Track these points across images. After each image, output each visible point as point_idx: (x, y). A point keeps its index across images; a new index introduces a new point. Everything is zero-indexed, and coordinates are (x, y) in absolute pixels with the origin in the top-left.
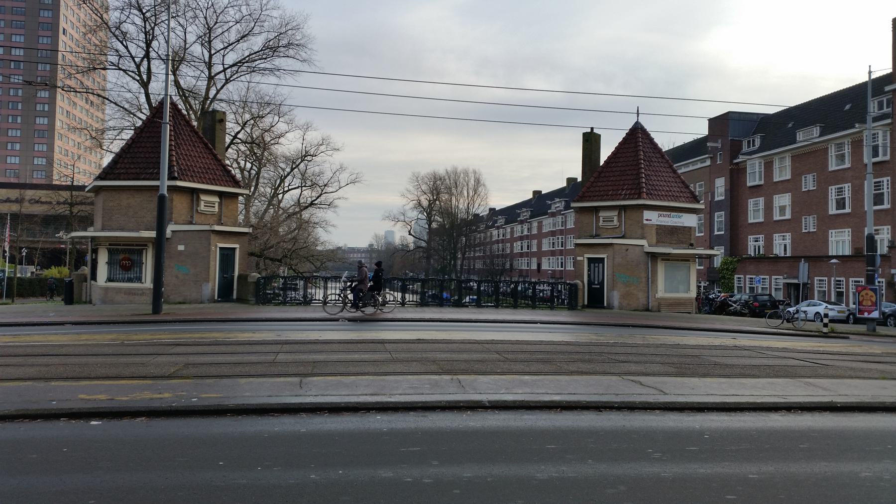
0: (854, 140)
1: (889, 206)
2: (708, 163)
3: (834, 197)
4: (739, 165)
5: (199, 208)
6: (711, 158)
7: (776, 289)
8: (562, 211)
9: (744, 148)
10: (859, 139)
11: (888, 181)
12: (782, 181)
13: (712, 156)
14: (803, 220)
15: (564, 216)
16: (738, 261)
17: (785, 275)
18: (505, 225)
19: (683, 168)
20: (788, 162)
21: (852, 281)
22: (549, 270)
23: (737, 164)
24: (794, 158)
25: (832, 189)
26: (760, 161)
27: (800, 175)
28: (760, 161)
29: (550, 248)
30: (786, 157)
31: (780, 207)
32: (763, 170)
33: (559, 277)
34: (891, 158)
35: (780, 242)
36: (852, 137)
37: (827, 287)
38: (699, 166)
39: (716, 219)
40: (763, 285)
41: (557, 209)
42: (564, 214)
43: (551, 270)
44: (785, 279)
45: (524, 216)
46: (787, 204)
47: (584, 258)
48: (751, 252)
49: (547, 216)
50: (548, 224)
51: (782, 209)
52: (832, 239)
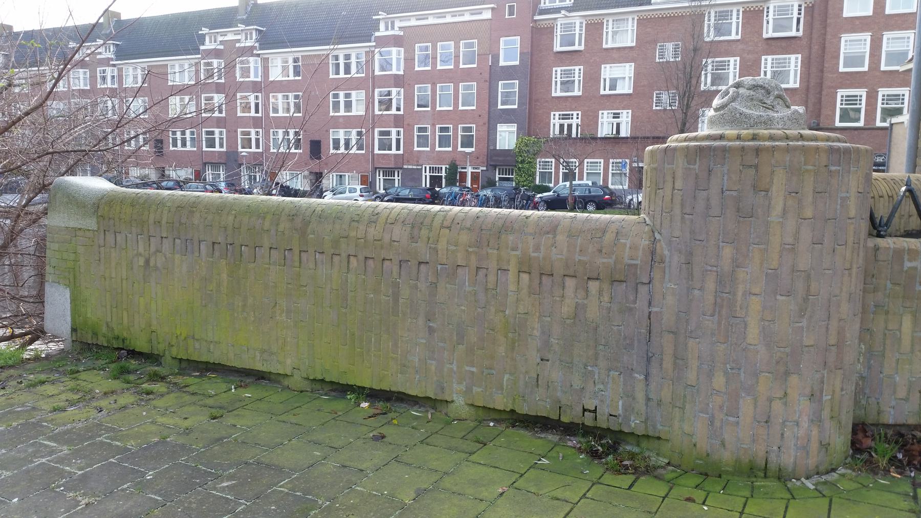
1: (580, 93)
2: (487, 15)
3: (559, 79)
4: (538, 23)
11: (580, 70)
12: (619, 49)
13: (496, 7)
18: (261, 49)
23: (536, 21)
25: (556, 71)
26: (581, 21)
27: (655, 42)
28: (581, 21)
30: (628, 19)
31: (611, 79)
34: (803, 34)
35: (608, 120)
36: (746, 6)
48: (554, 131)
52: (602, 120)
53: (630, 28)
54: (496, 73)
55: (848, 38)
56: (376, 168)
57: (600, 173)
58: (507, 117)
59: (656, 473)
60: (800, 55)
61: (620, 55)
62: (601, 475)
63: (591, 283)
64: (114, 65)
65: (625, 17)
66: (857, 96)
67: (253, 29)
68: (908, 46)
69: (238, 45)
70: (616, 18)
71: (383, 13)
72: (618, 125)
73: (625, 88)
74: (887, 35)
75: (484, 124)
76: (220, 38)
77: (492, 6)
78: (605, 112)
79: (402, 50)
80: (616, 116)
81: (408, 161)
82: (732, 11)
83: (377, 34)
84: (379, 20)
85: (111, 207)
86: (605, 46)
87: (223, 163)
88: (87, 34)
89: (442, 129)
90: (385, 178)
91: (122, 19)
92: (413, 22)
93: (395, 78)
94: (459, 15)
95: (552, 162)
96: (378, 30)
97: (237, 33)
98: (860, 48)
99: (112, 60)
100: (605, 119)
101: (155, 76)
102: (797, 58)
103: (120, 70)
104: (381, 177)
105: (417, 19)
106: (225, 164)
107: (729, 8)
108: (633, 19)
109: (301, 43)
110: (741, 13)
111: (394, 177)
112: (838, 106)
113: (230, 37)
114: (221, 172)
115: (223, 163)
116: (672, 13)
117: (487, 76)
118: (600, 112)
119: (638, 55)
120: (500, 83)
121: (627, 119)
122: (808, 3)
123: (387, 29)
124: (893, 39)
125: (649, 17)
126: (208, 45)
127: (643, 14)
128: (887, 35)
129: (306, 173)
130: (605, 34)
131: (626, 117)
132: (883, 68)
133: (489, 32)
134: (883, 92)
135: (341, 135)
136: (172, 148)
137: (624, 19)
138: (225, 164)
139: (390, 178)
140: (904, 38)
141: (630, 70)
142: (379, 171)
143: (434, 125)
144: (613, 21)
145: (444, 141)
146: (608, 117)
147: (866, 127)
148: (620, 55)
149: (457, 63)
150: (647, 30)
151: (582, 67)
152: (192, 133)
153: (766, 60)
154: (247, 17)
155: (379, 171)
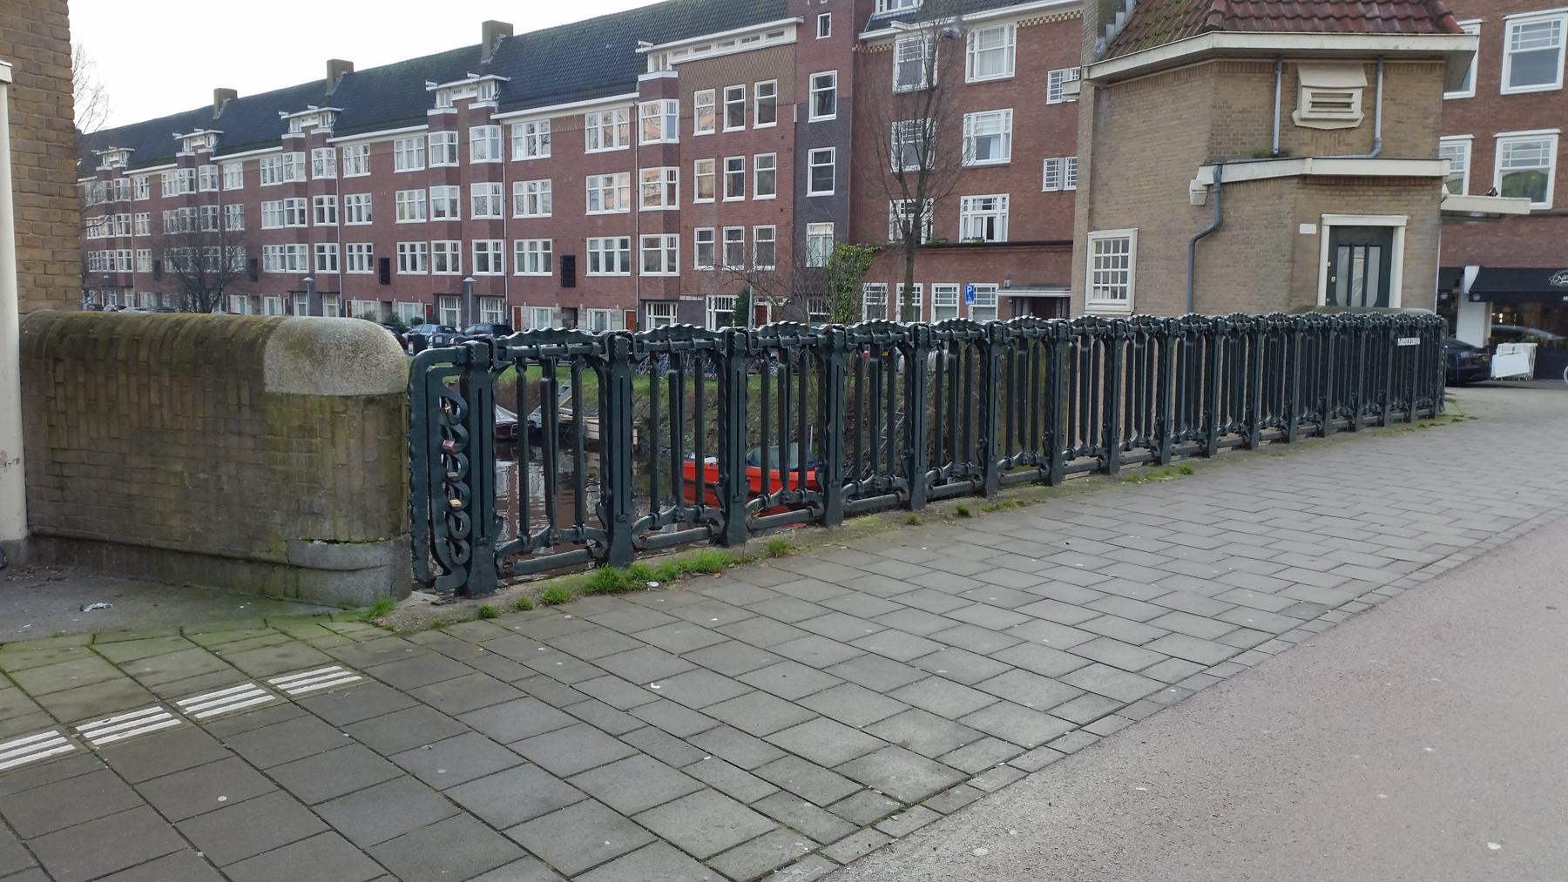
0: (1024, 25)
2: (790, 36)
4: (869, 45)
5: (1295, 115)
6: (798, 25)
7: (937, 309)
8: (125, 170)
9: (878, 8)
10: (1066, 18)
12: (989, 83)
13: (802, 21)
14: (1045, 166)
15: (499, 128)
16: (876, 253)
17: (1008, 282)
18: (501, 111)
19: (310, 119)
20: (1008, 40)
21: (937, 289)
22: (105, 274)
23: (865, 42)
24: (1024, 34)
27: (1043, 70)
29: (282, 222)
30: (1003, 30)
32: (1014, 44)
33: (124, 285)
35: (974, 212)
37: (921, 301)
38: (764, 42)
39: (811, 164)
40: (979, 302)
41: (115, 166)
42: (217, 161)
43: (109, 274)
44: (1007, 288)
45: (112, 163)
46: (1002, 132)
47: (1320, 227)
49: (176, 165)
50: (282, 166)
51: (984, 146)
52: (965, 213)
53: (1006, 45)
54: (804, 135)
55: (1520, 23)
56: (644, 301)
57: (995, 308)
58: (820, 211)
60: (1012, 109)
61: (992, 95)
63: (62, 381)
64: (331, 145)
65: (998, 26)
67: (328, 111)
68: (1556, 41)
69: (472, 106)
70: (984, 27)
71: (312, 107)
72: (991, 221)
73: (1000, 155)
74: (1513, 22)
75: (788, 223)
76: (672, 59)
77: (794, 19)
78: (970, 198)
79: (677, 102)
80: (987, 206)
81: (686, 289)
83: (642, 78)
84: (646, 54)
86: (968, 80)
87: (458, 295)
88: (453, 65)
89: (731, 234)
90: (657, 316)
91: (355, 70)
92: (691, 56)
93: (664, 150)
94: (753, 39)
95: (955, 289)
96: (645, 71)
97: (313, 116)
98: (1547, 43)
99: (328, 135)
100: (970, 212)
101: (567, 137)
102: (1008, 114)
103: (340, 151)
104: (485, 310)
105: (697, 50)
106: (461, 295)
108: (1011, 28)
109: (546, 99)
110: (1015, 31)
111: (669, 315)
113: (465, 95)
114: (671, 316)
115: (458, 295)
116: (1072, 13)
117: (790, 140)
118: (963, 198)
119: (1019, 93)
120: (811, 152)
121: (1004, 211)
122: (1057, 16)
123: (657, 69)
124: (1526, 28)
125: (1035, 23)
126: (441, 108)
127: (1026, 18)
128: (1513, 22)
129: (557, 309)
130: (968, 58)
131: (1001, 207)
132: (1506, 88)
133: (793, 65)
135: (599, 245)
136: (590, 273)
137: (997, 30)
138: (461, 295)
139: (663, 317)
140: (1547, 25)
141: (1007, 121)
142: (650, 306)
143: (719, 228)
144: (981, 34)
145: (736, 253)
146: (974, 208)
147: (1558, 210)
148: (992, 95)
149: (719, 125)
150: (1032, 47)
152: (624, 244)
154: (492, 61)
155: (650, 306)
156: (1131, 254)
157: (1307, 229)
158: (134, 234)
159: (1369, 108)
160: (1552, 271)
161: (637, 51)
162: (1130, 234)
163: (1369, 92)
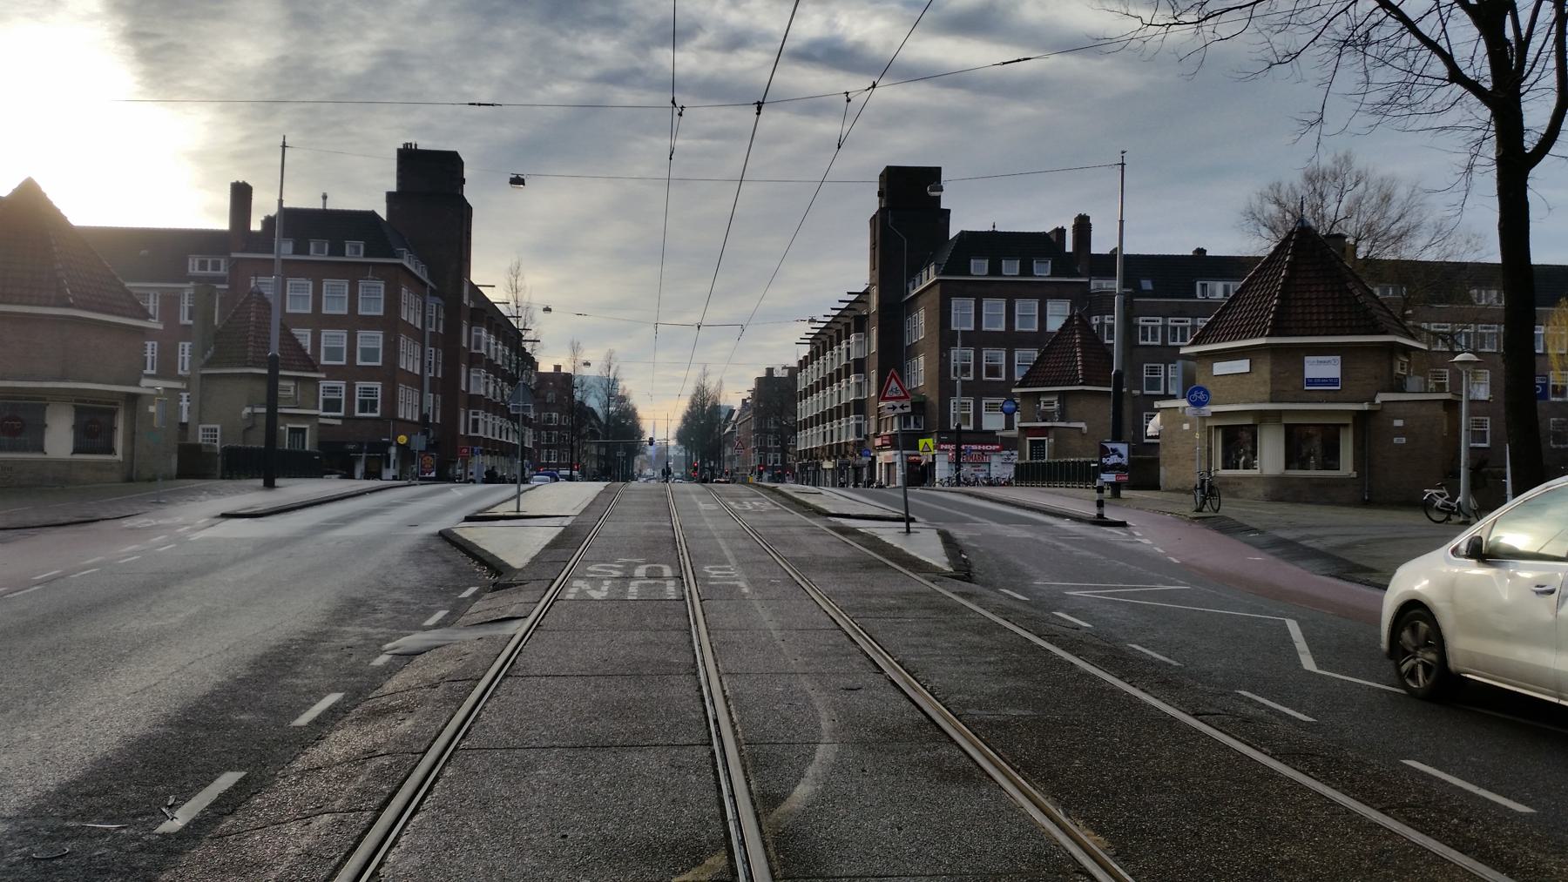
59: (801, 387)
62: (491, 103)
66: (373, 389)
82: (148, 295)
85: (1367, 31)
107: (146, 292)
110: (158, 298)
112: (357, 397)
124: (366, 337)
134: (359, 385)
151: (156, 343)
153: (183, 346)
156: (218, 433)
157: (282, 428)
158: (278, 256)
159: (296, 391)
160: (345, 443)
161: (1069, 248)
162: (218, 427)
163: (296, 387)
